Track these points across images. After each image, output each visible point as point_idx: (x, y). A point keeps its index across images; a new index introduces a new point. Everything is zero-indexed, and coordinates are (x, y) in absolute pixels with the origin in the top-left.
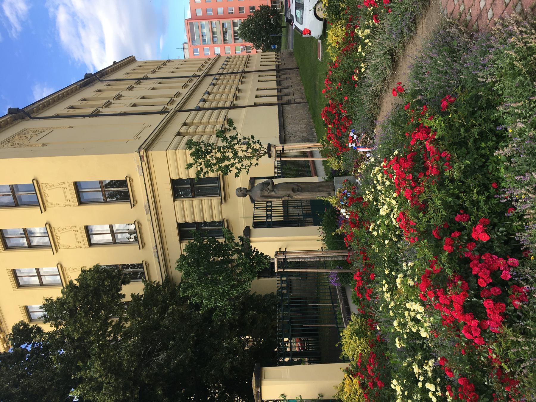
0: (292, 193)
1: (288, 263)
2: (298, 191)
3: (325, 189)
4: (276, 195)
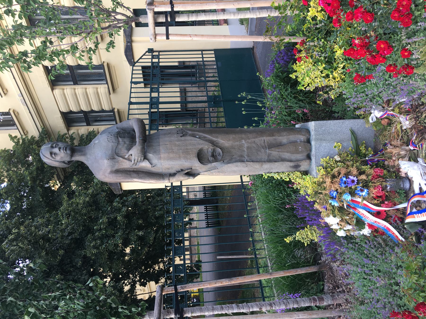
0: (196, 165)
1: (186, 248)
2: (215, 158)
3: (286, 155)
4: (154, 170)
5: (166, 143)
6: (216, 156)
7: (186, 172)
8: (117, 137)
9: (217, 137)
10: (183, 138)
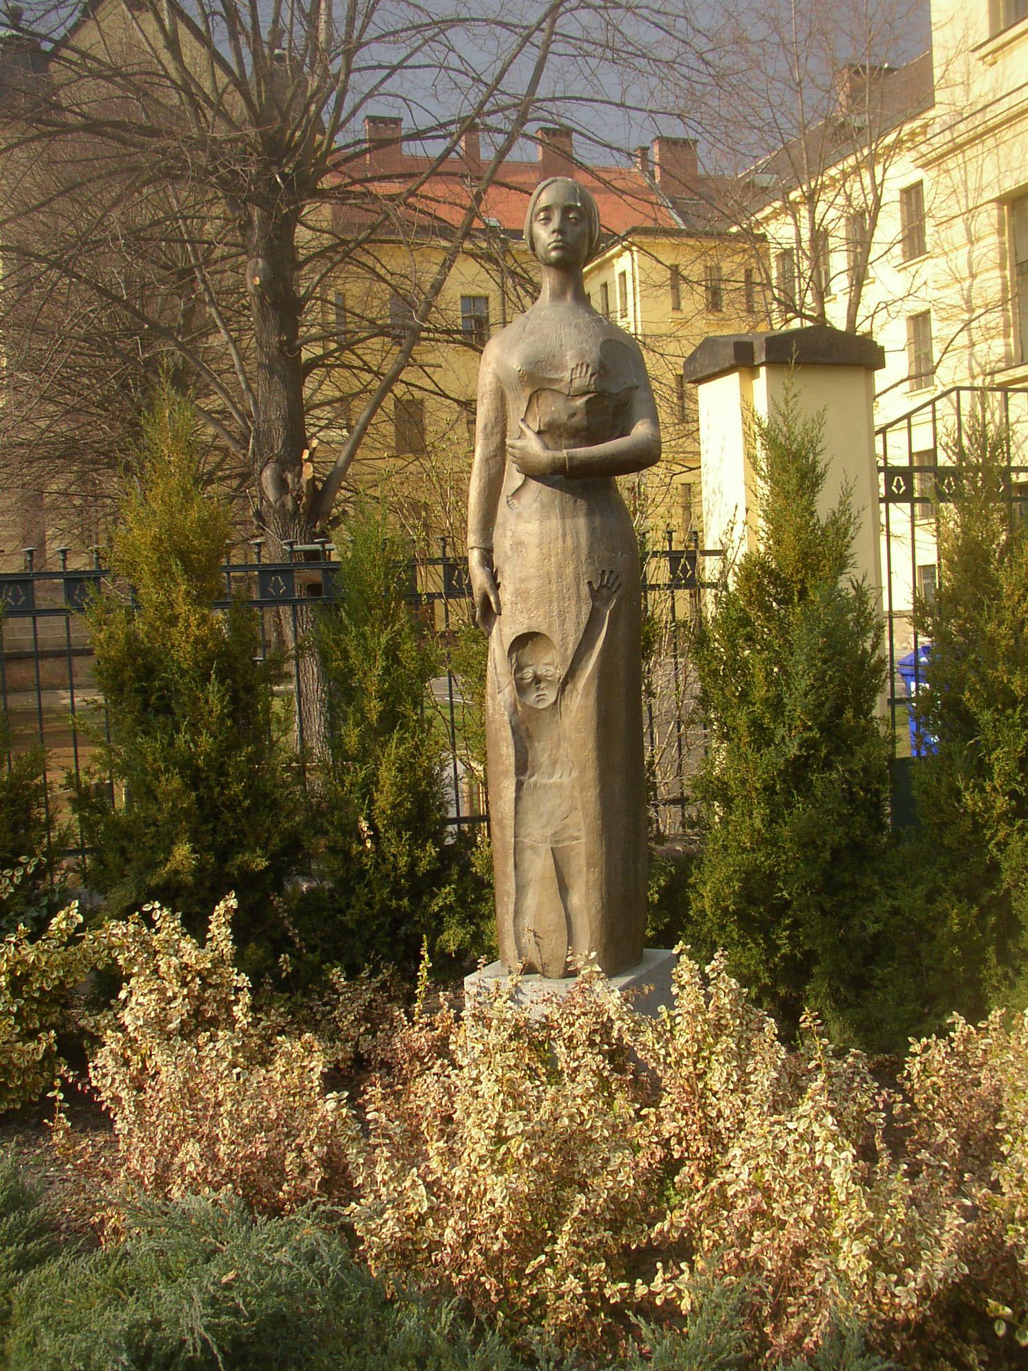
5: (568, 537)
6: (538, 689)
7: (492, 599)
8: (587, 393)
9: (586, 694)
10: (585, 589)
